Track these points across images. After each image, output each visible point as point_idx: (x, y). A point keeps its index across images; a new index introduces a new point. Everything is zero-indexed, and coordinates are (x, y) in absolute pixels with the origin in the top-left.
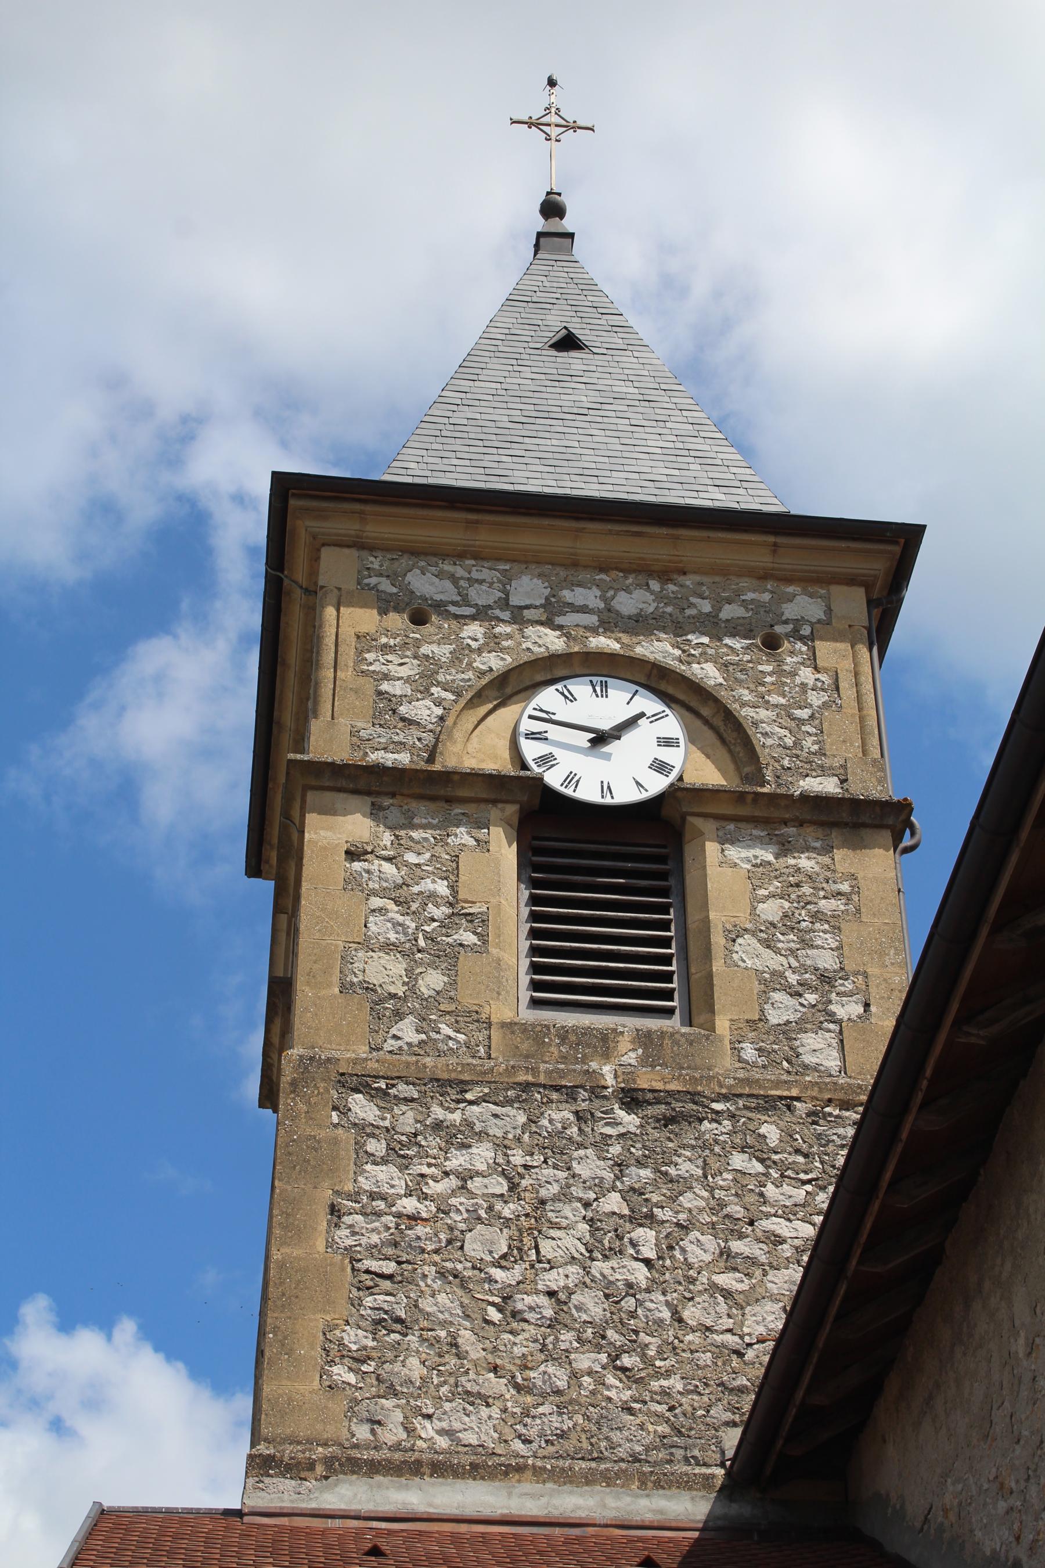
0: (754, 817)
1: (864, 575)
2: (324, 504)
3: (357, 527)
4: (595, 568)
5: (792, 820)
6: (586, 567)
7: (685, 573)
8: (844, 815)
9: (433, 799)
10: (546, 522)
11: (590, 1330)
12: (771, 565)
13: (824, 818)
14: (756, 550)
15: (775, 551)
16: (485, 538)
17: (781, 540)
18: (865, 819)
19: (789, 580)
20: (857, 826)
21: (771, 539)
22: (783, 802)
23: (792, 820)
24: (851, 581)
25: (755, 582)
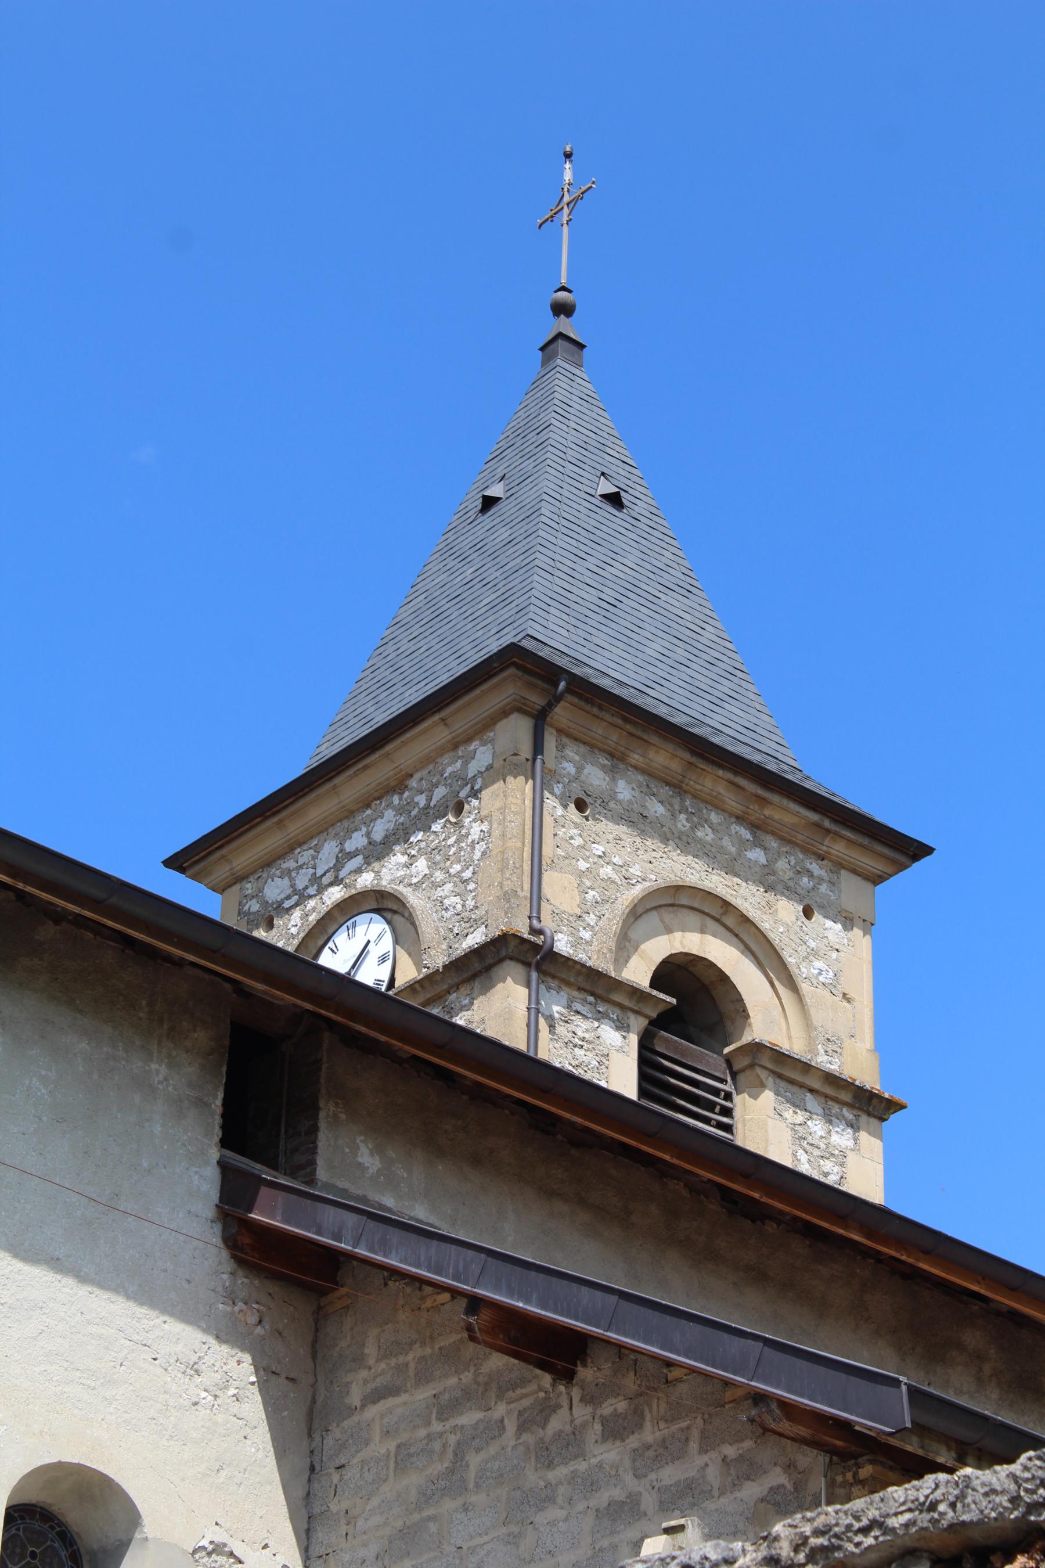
0: (429, 999)
1: (507, 705)
2: (202, 864)
3: (228, 868)
4: (363, 807)
5: (451, 988)
6: (358, 810)
7: (411, 776)
8: (476, 965)
9: (780, 1076)
10: (313, 795)
11: (145, 1164)
12: (450, 737)
13: (465, 975)
14: (432, 734)
15: (446, 724)
16: (294, 828)
17: (443, 714)
18: (490, 961)
19: (469, 740)
20: (489, 968)
21: (437, 717)
22: (438, 978)
23: (451, 988)
24: (504, 713)
25: (452, 754)
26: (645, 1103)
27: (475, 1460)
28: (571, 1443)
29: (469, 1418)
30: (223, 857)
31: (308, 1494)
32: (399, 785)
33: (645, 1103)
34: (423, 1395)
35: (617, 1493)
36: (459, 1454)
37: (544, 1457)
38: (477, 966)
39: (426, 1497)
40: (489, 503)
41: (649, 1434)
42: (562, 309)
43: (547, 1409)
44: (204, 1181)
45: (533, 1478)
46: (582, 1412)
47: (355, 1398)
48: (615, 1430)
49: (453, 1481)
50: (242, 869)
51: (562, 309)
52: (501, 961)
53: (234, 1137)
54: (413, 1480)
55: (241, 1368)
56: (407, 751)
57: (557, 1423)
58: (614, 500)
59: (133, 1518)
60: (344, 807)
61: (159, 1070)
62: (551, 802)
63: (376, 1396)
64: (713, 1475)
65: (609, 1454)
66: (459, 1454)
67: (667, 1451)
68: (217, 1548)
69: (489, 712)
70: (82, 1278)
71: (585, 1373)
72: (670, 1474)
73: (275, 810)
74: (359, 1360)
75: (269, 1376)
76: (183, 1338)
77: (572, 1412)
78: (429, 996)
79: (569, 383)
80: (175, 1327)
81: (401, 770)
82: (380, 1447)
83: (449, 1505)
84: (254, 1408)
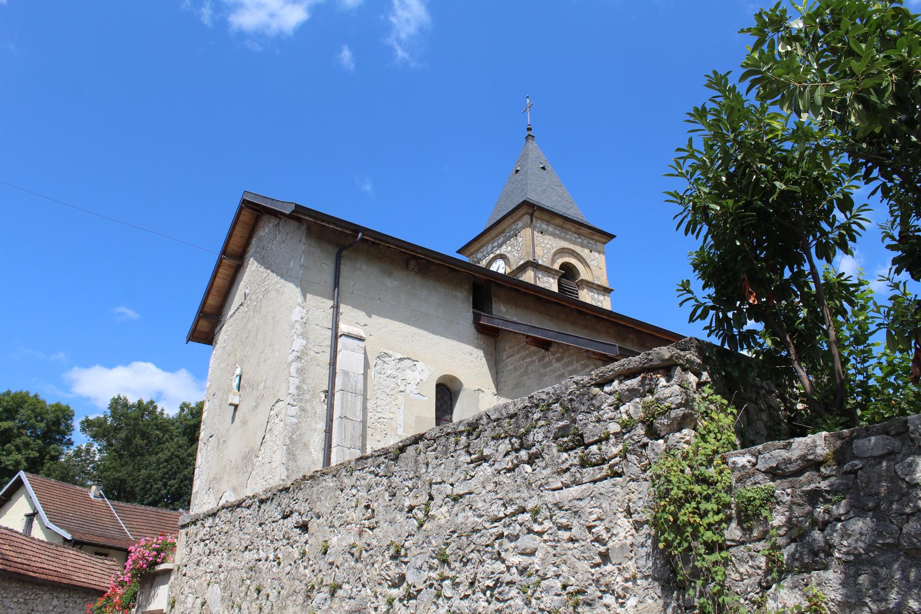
27: (530, 368)
28: (550, 363)
29: (528, 360)
34: (518, 356)
35: (560, 373)
36: (527, 367)
37: (544, 366)
39: (521, 376)
40: (517, 171)
41: (565, 360)
42: (529, 129)
43: (544, 357)
44: (470, 316)
45: (542, 371)
46: (551, 357)
47: (504, 358)
48: (558, 360)
49: (526, 373)
51: (529, 129)
53: (475, 306)
54: (518, 373)
55: (480, 353)
57: (546, 360)
58: (543, 168)
59: (462, 385)
61: (458, 294)
62: (343, 308)
63: (509, 357)
64: (579, 367)
65: (558, 365)
66: (527, 367)
67: (570, 363)
68: (479, 390)
70: (447, 338)
71: (551, 349)
72: (570, 368)
74: (505, 350)
75: (486, 354)
76: (468, 348)
77: (549, 357)
79: (532, 145)
80: (466, 346)
82: (511, 367)
83: (525, 378)
84: (484, 361)
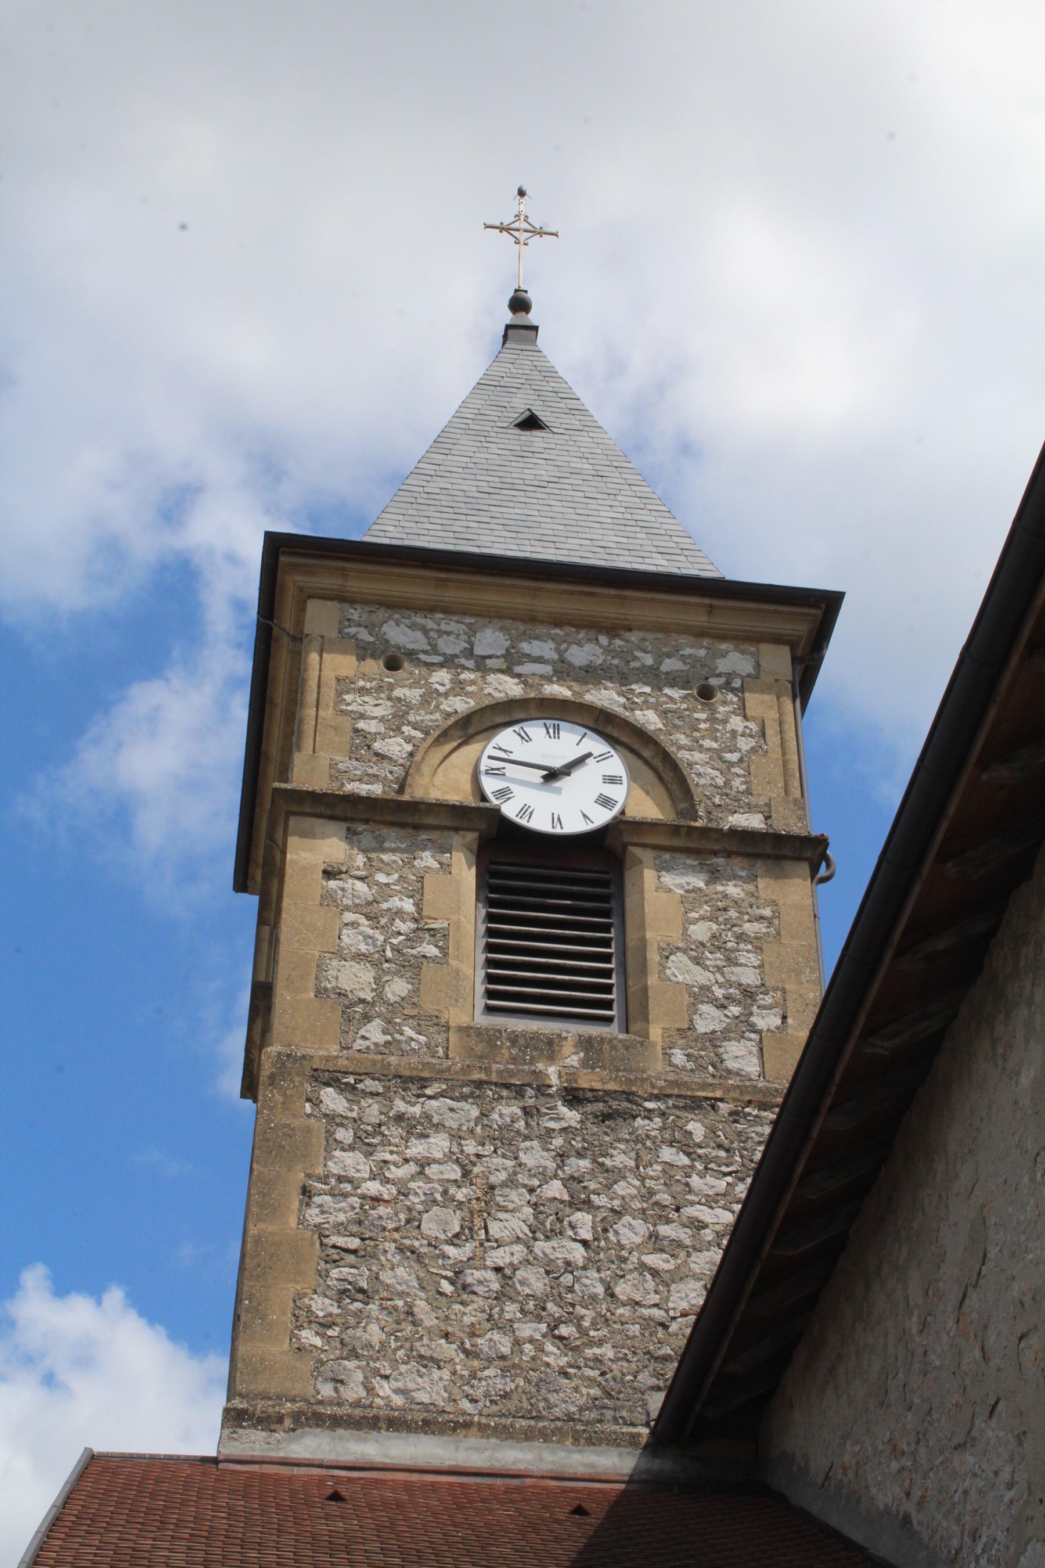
2: (311, 561)
4: (550, 623)
10: (498, 580)
13: (748, 850)
16: (452, 595)
17: (716, 602)
18: (785, 851)
19: (723, 638)
21: (707, 601)
24: (777, 640)
26: (254, 1443)
30: (344, 569)
31: (984, 1223)
32: (613, 630)
33: (254, 1443)
38: (768, 849)
50: (449, 602)
52: (800, 859)
56: (640, 608)
60: (533, 611)
69: (764, 630)
73: (308, 552)
78: (691, 845)
81: (627, 620)
